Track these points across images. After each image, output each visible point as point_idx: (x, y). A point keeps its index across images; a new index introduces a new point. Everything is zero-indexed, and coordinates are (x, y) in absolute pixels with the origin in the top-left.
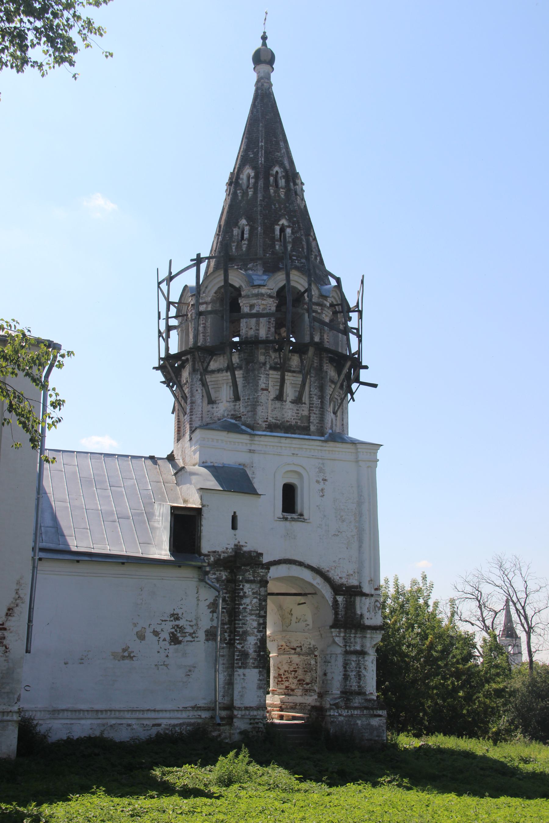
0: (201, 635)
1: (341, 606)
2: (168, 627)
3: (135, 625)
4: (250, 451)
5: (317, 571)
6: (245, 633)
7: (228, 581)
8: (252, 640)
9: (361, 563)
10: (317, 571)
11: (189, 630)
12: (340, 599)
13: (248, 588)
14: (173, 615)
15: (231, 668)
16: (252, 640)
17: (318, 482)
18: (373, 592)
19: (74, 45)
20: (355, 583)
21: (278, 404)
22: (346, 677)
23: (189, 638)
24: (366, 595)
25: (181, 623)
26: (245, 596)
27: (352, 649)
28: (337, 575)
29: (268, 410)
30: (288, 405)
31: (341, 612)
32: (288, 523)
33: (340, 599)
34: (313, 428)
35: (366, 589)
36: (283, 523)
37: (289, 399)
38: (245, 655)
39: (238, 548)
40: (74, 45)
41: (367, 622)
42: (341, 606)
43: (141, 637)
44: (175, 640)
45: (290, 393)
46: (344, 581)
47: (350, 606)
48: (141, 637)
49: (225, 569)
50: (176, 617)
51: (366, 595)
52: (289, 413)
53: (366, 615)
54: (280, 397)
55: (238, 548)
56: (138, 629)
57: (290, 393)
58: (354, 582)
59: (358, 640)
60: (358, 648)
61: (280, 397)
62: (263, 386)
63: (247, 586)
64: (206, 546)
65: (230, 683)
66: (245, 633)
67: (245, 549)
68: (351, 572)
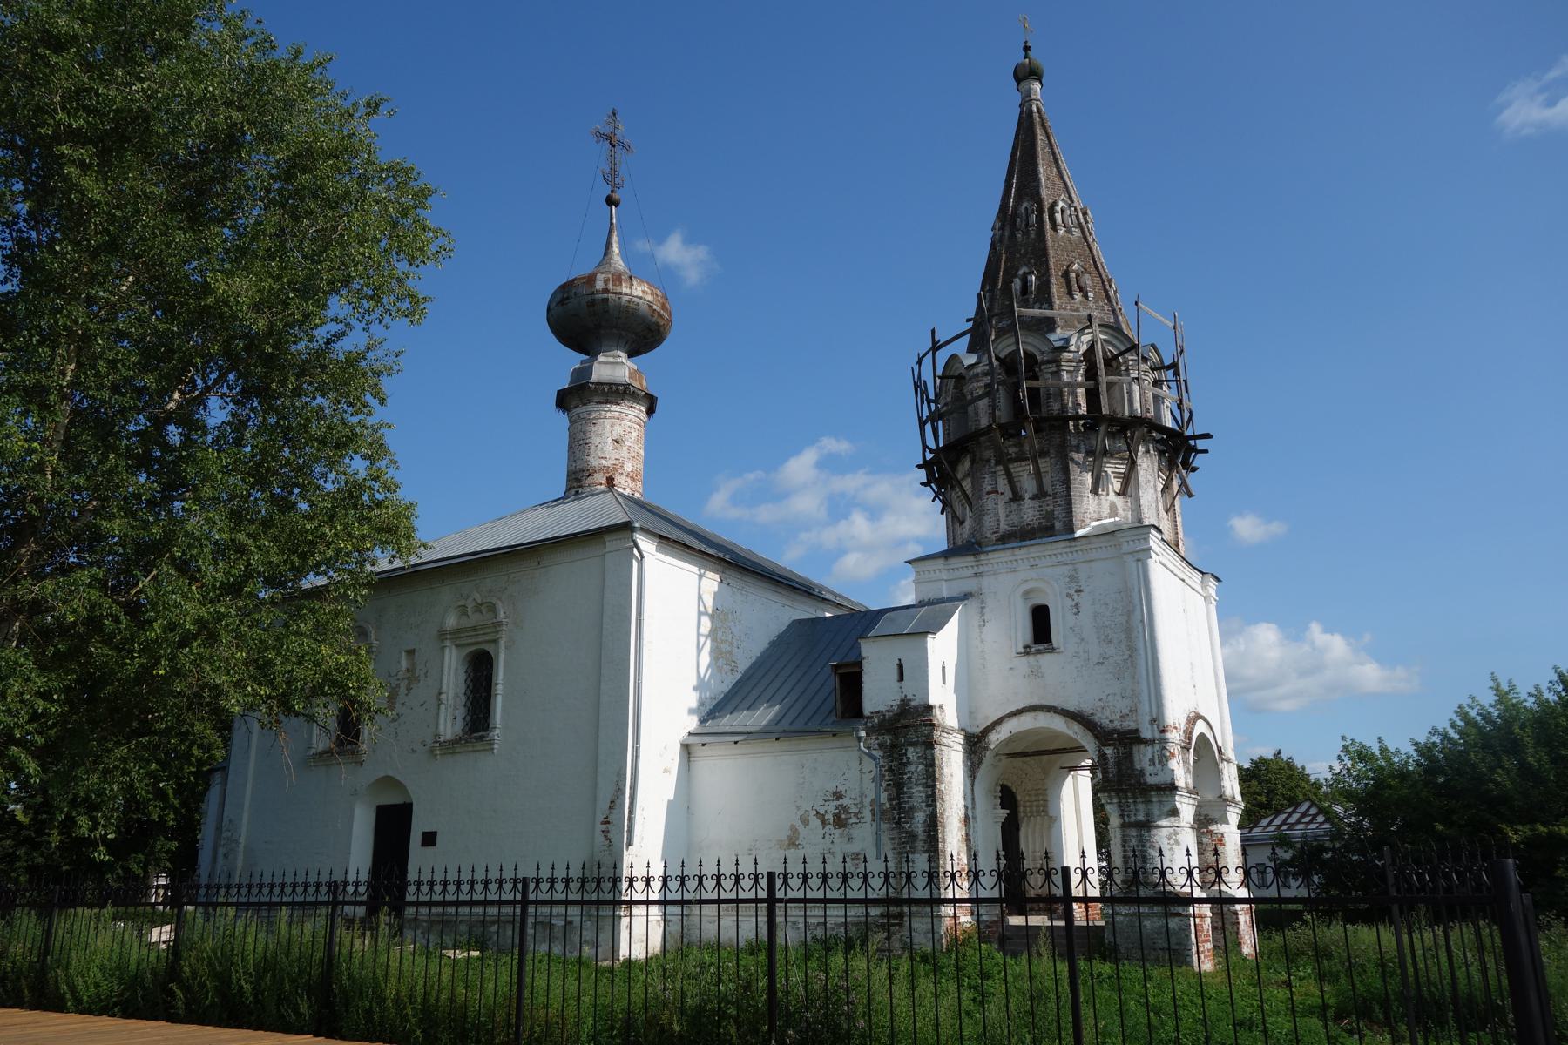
0: (867, 814)
1: (1111, 762)
2: (831, 808)
3: (798, 808)
4: (976, 575)
5: (1065, 713)
6: (912, 809)
7: (893, 746)
8: (920, 818)
10: (1065, 713)
11: (854, 810)
12: (1109, 751)
13: (911, 753)
14: (834, 793)
16: (920, 818)
17: (1069, 595)
18: (1157, 735)
20: (1133, 726)
21: (1014, 506)
23: (854, 820)
24: (1146, 742)
25: (845, 802)
26: (909, 763)
27: (1133, 819)
28: (1103, 718)
29: (998, 514)
30: (1028, 503)
31: (1112, 770)
32: (1031, 658)
33: (1109, 751)
34: (1058, 525)
35: (1146, 733)
36: (1024, 659)
37: (1027, 496)
38: (912, 836)
39: (905, 702)
41: (1151, 780)
42: (1111, 762)
43: (805, 821)
44: (839, 822)
45: (1028, 486)
46: (1116, 725)
47: (1126, 759)
48: (805, 821)
49: (127, 801)
50: (838, 795)
51: (1146, 742)
52: (1030, 512)
53: (1149, 769)
54: (1017, 497)
55: (905, 702)
56: (801, 813)
57: (1028, 486)
59: (1141, 807)
60: (1141, 817)
61: (1017, 497)
62: (989, 488)
63: (911, 749)
64: (868, 707)
65: (48, 933)
66: (912, 809)
68: (1126, 711)
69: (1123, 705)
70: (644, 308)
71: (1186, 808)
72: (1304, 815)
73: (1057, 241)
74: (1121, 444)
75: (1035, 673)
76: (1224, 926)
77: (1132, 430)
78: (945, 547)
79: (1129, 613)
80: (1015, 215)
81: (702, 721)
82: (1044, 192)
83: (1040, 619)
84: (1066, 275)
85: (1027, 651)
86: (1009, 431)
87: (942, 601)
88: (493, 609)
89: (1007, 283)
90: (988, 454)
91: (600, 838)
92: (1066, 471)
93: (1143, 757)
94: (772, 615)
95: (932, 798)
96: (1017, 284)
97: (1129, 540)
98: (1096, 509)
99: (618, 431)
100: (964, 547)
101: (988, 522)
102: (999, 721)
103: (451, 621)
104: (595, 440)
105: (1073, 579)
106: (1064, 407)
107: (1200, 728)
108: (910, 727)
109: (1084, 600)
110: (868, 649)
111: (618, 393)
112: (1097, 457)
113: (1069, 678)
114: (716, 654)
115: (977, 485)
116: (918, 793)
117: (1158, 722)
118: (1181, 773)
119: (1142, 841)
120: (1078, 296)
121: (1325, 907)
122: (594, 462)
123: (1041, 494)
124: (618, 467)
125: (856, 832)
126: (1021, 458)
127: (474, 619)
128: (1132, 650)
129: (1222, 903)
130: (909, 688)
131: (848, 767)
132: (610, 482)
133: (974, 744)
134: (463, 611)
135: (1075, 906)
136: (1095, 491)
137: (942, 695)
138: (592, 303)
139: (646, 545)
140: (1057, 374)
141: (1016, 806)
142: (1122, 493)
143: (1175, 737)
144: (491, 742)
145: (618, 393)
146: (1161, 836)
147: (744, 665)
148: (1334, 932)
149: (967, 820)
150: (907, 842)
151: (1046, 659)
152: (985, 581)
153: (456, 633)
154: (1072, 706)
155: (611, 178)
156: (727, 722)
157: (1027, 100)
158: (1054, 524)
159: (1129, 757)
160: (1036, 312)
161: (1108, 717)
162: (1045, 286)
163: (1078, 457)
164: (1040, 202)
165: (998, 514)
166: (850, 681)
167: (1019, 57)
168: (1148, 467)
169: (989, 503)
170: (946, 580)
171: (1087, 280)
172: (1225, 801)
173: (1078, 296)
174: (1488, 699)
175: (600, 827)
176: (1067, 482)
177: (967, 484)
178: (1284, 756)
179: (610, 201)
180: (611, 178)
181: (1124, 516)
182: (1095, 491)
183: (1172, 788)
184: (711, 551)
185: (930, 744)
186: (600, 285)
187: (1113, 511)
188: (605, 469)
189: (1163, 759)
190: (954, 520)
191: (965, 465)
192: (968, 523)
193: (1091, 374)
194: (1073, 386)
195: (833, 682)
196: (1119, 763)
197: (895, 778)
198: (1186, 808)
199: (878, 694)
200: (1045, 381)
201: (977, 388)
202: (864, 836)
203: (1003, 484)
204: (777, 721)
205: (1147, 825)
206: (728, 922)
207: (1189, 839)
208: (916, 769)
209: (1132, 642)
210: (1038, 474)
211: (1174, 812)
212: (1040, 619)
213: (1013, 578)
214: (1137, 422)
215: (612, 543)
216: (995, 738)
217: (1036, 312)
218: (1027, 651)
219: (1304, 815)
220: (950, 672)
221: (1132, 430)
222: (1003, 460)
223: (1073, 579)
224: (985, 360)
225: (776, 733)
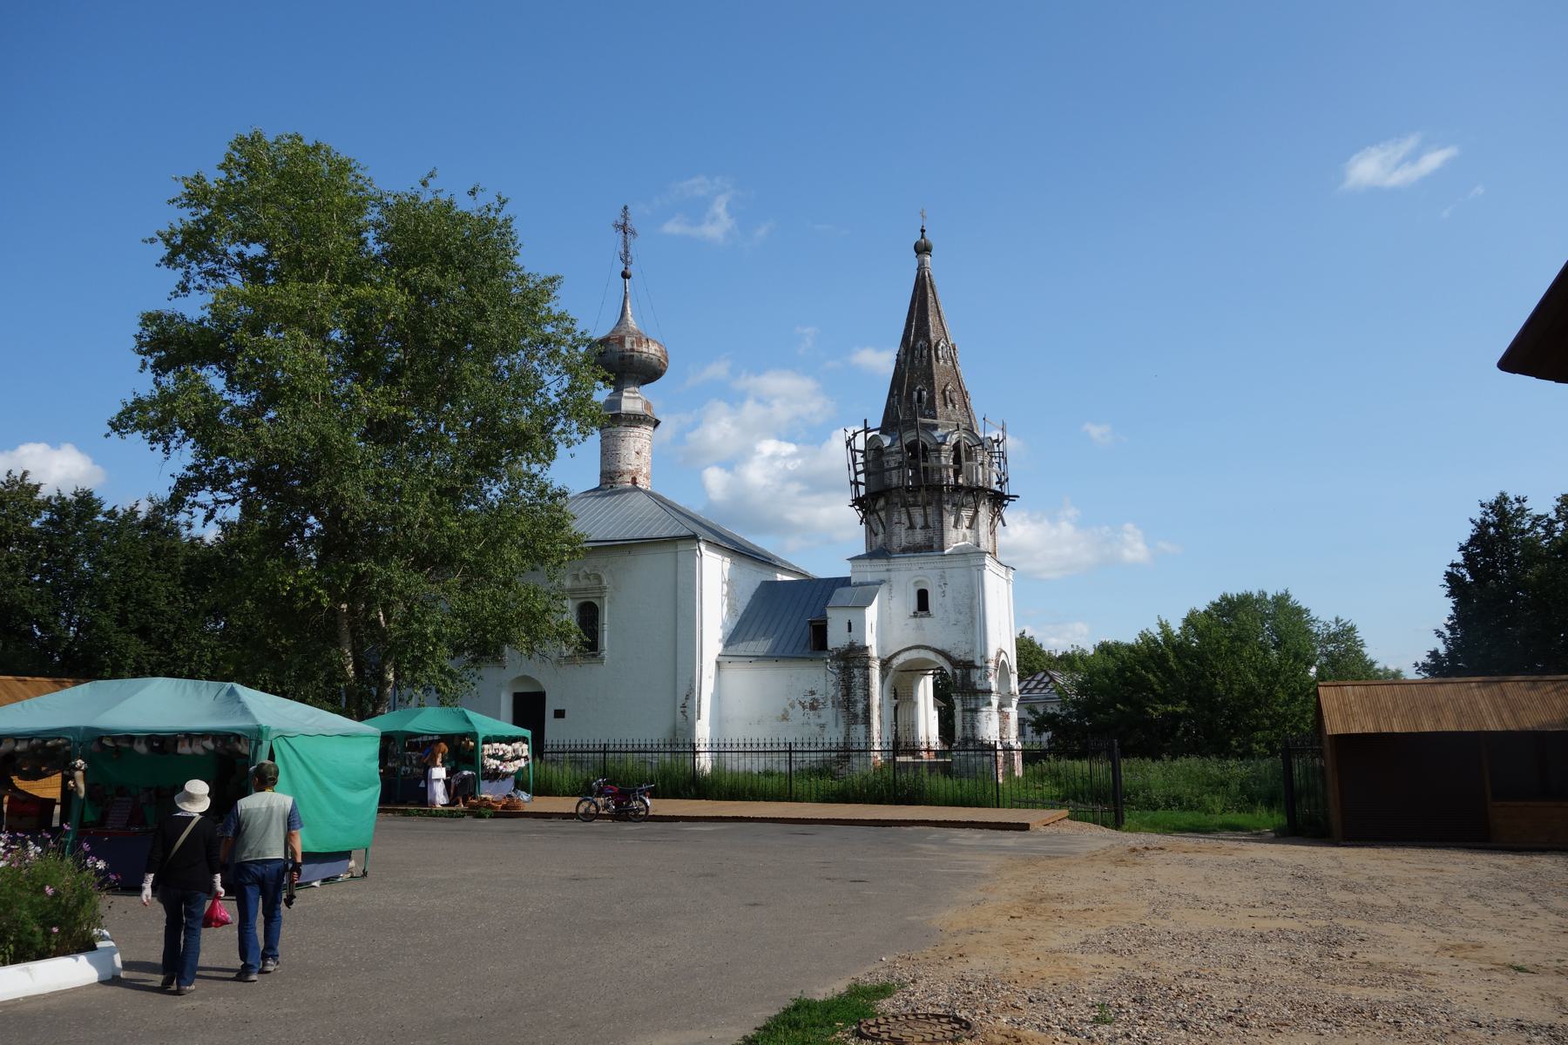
2: (808, 700)
5: (927, 648)
8: (860, 706)
9: (973, 643)
13: (856, 671)
15: (848, 725)
19: (1269, 598)
22: (964, 728)
28: (956, 654)
29: (901, 536)
35: (978, 663)
38: (856, 716)
39: (852, 644)
40: (1269, 598)
43: (793, 706)
44: (813, 707)
45: (919, 521)
47: (967, 676)
48: (793, 706)
50: (812, 693)
52: (919, 536)
54: (912, 527)
55: (852, 644)
58: (969, 658)
61: (912, 527)
64: (830, 645)
67: (1377, 666)
69: (967, 648)
70: (655, 361)
71: (995, 700)
72: (1039, 682)
73: (939, 367)
74: (971, 499)
75: (919, 628)
76: (1009, 761)
77: (976, 493)
78: (863, 552)
79: (972, 598)
80: (914, 348)
81: (725, 646)
82: (932, 335)
83: (923, 597)
84: (944, 392)
85: (915, 615)
86: (914, 490)
87: (868, 584)
88: (599, 578)
89: (910, 395)
90: (896, 500)
91: (679, 715)
92: (941, 515)
93: (976, 675)
94: (755, 577)
95: (867, 696)
96: (915, 395)
97: (973, 557)
98: (956, 537)
99: (638, 446)
100: (878, 552)
101: (895, 540)
102: (899, 653)
103: (568, 583)
104: (623, 452)
105: (942, 577)
106: (941, 479)
107: (1003, 657)
108: (854, 657)
109: (948, 589)
110: (830, 613)
111: (636, 420)
112: (959, 507)
113: (939, 631)
114: (729, 605)
115: (889, 517)
116: (859, 693)
117: (984, 657)
118: (993, 684)
119: (973, 719)
120: (950, 406)
121: (1061, 749)
122: (623, 467)
123: (926, 527)
124: (638, 471)
125: (822, 713)
126: (915, 505)
127: (584, 583)
128: (973, 618)
129: (1008, 749)
130: (854, 636)
131: (819, 678)
132: (634, 481)
133: (885, 664)
134: (576, 577)
135: (57, 779)
136: (955, 526)
137: (871, 640)
138: (622, 358)
139: (703, 546)
140: (938, 458)
141: (902, 696)
142: (969, 528)
143: (992, 665)
144: (602, 659)
145: (636, 420)
146: (982, 716)
147: (741, 611)
148: (1064, 763)
149: (880, 706)
150: (852, 719)
151: (926, 621)
152: (893, 574)
153: (572, 591)
154: (939, 646)
155: (625, 258)
156: (741, 648)
157: (921, 267)
158: (932, 546)
159: (968, 675)
160: (929, 421)
161: (958, 654)
162: (932, 399)
163: (948, 507)
164: (929, 342)
165: (901, 536)
166: (819, 632)
167: (918, 237)
168: (984, 512)
169: (896, 529)
170: (871, 571)
171: (956, 396)
172: (1011, 695)
173: (950, 406)
174: (1155, 630)
175: (679, 710)
176: (941, 522)
177: (882, 514)
178: (1027, 635)
179: (625, 275)
180: (625, 258)
181: (970, 542)
182: (955, 526)
183: (990, 692)
184: (724, 544)
185: (867, 667)
186: (628, 346)
187: (965, 538)
188: (630, 472)
189: (986, 677)
190: (871, 533)
191: (882, 502)
192: (881, 537)
193: (957, 460)
194: (947, 467)
195: (808, 631)
196: (963, 678)
197: (847, 687)
198: (995, 700)
199: (837, 638)
200: (932, 462)
201: (893, 461)
202: (828, 714)
203: (904, 518)
204: (774, 648)
205: (976, 711)
206: (748, 760)
207: (995, 717)
208: (858, 680)
209: (972, 613)
210: (925, 516)
211: (990, 704)
212: (923, 597)
213: (907, 574)
214: (982, 489)
215: (682, 547)
216: (896, 662)
217: (929, 421)
218: (915, 615)
219: (1039, 682)
220: (878, 626)
221: (976, 493)
222: (906, 505)
223: (942, 577)
224: (898, 444)
225: (772, 657)
